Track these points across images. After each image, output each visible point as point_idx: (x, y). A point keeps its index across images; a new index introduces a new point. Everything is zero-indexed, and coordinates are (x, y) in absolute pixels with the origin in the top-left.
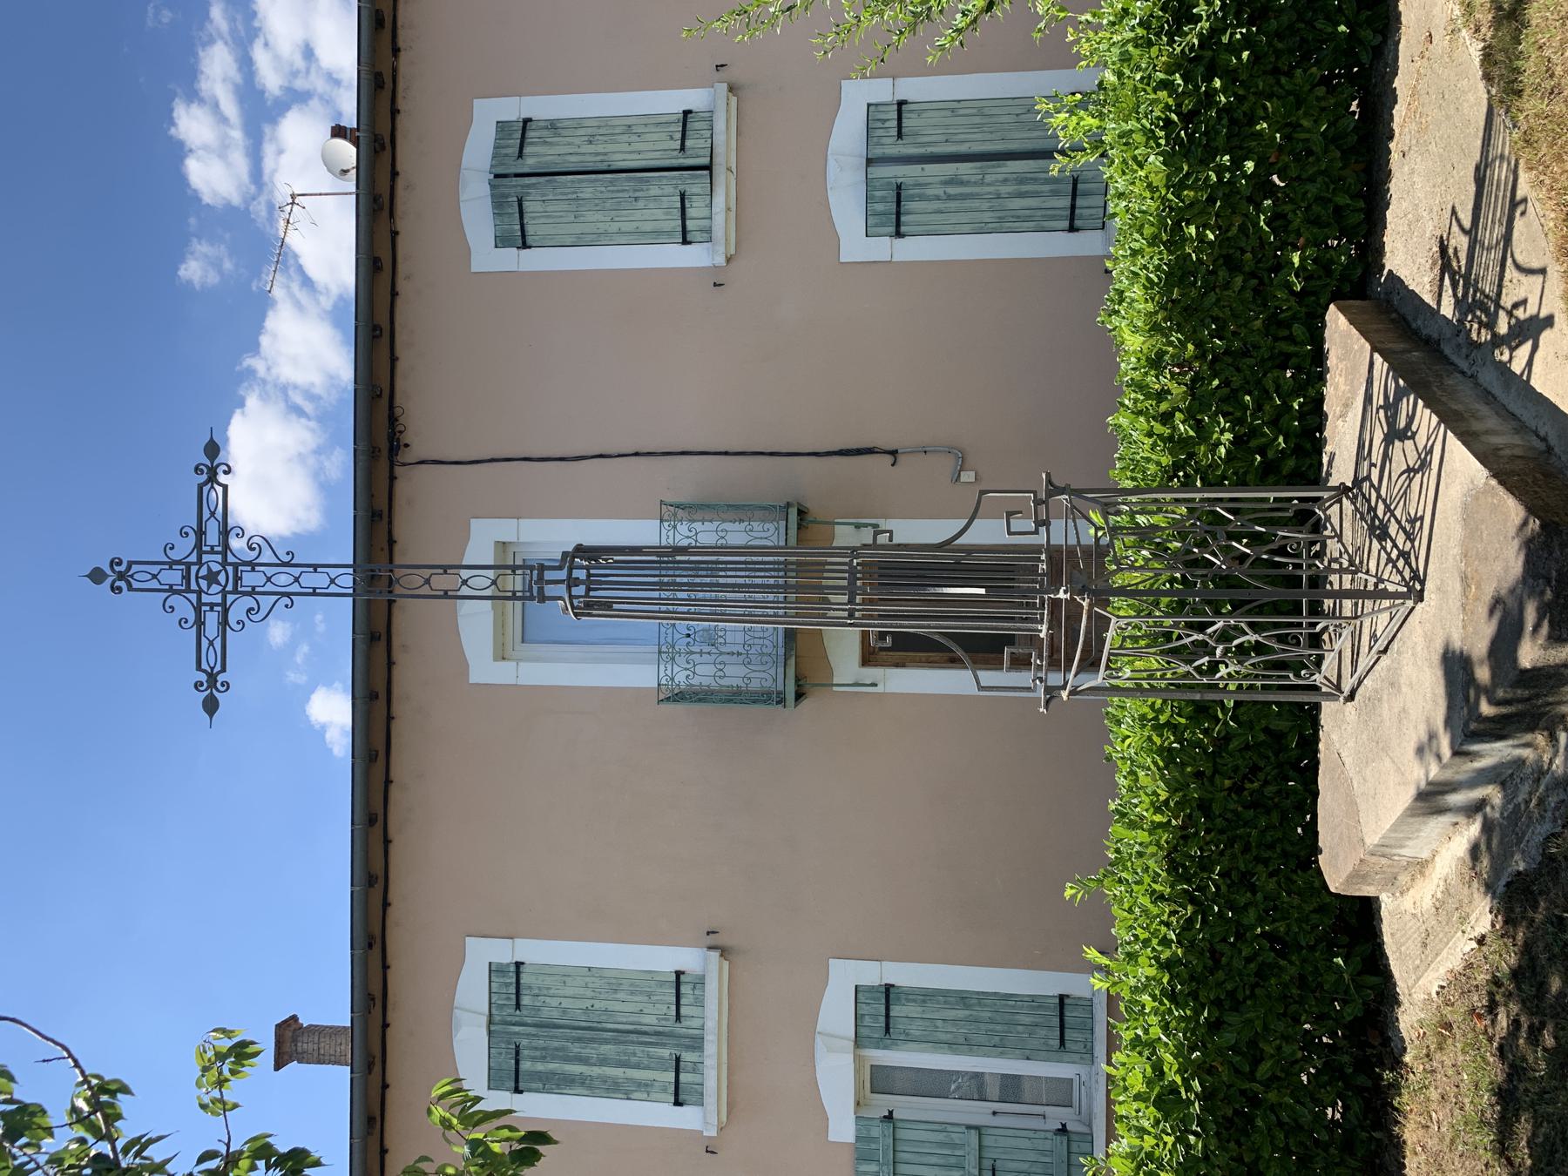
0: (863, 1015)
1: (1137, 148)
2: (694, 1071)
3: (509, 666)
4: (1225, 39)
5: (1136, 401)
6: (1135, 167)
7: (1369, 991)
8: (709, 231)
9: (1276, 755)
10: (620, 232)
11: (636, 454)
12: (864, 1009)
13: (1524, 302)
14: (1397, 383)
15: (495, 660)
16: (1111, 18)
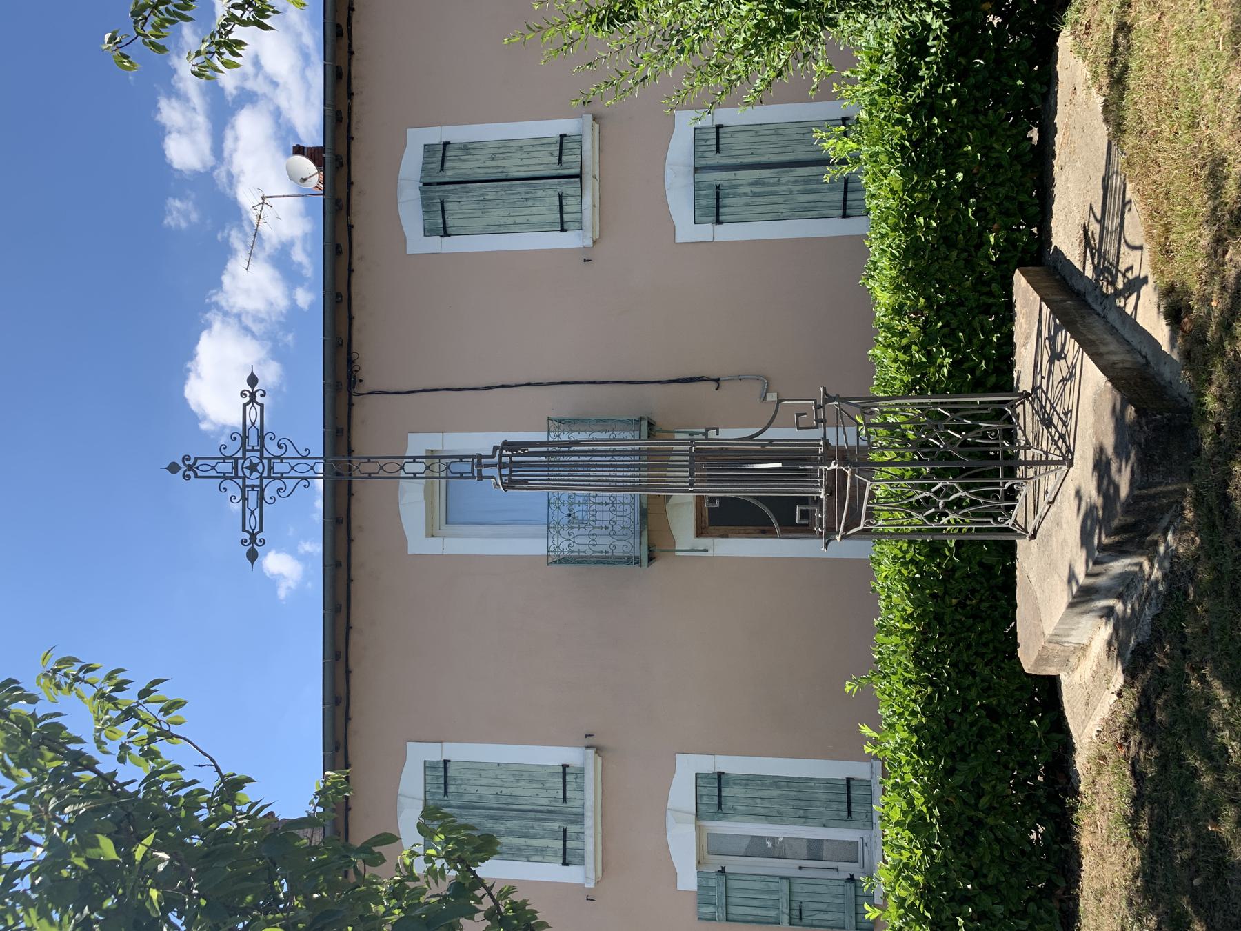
0: (701, 796)
1: (883, 164)
2: (577, 839)
3: (437, 541)
4: (940, 91)
5: (885, 338)
6: (882, 177)
7: (1056, 744)
8: (580, 222)
9: (988, 581)
10: (515, 224)
11: (529, 384)
12: (702, 791)
13: (1131, 268)
14: (1055, 322)
15: (427, 536)
16: (863, 76)
